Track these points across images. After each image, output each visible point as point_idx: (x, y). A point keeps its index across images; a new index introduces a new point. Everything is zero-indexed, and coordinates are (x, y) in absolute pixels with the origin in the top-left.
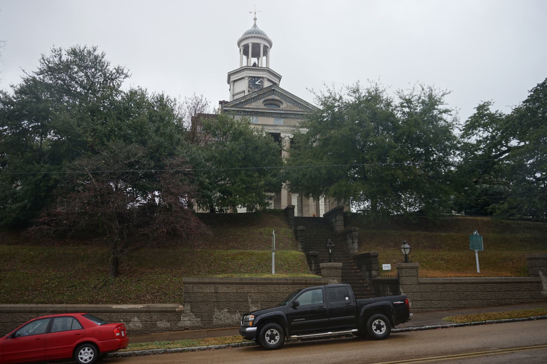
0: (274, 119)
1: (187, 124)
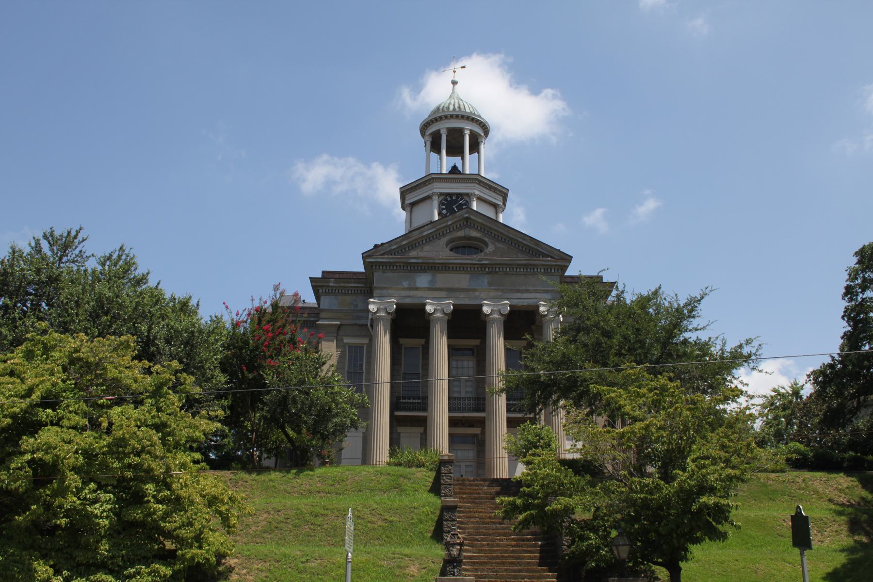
0: (468, 276)
1: (309, 298)
